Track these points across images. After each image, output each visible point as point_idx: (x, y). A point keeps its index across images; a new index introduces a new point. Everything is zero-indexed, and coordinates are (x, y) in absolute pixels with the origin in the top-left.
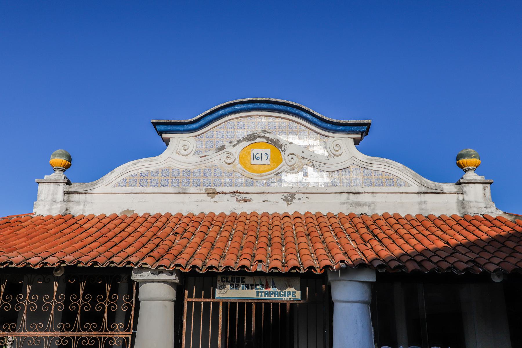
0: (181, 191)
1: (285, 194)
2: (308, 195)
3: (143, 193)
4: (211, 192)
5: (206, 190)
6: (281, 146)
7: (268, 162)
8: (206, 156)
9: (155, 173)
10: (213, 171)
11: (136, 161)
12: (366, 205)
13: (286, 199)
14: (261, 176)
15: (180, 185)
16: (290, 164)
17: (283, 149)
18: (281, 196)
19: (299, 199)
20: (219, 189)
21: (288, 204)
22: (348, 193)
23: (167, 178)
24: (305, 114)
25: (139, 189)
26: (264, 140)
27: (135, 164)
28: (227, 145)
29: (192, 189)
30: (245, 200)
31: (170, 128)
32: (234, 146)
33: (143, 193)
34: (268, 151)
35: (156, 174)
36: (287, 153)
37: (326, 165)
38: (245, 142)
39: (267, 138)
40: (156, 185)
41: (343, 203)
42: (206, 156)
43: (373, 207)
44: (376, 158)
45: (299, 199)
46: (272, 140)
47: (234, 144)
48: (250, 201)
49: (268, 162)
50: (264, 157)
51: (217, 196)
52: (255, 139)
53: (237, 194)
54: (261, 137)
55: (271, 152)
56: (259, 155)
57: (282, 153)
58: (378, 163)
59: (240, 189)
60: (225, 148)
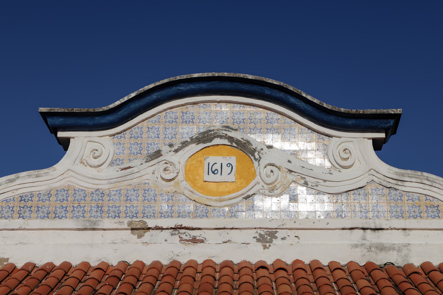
0: (88, 225)
1: (259, 231)
2: (298, 233)
3: (24, 229)
4: (138, 226)
5: (130, 224)
6: (252, 152)
7: (232, 178)
8: (130, 167)
9: (44, 195)
10: (141, 193)
11: (12, 176)
12: (394, 249)
13: (261, 239)
14: (221, 201)
15: (87, 215)
16: (269, 181)
17: (257, 157)
18: (253, 233)
19: (283, 239)
20: (151, 223)
21: (265, 247)
22: (364, 229)
23: (65, 204)
24: (292, 100)
25: (17, 223)
26: (226, 142)
27: (11, 181)
28: (165, 149)
29: (107, 223)
30: (194, 241)
31: (71, 121)
32: (176, 151)
33: (24, 229)
34: (233, 160)
35: (46, 197)
36: (263, 162)
37: (327, 183)
38: (194, 145)
39: (231, 139)
40: (47, 216)
41: (356, 246)
42: (130, 167)
43: (405, 252)
44: (409, 172)
45: (283, 239)
46: (238, 142)
47: (176, 147)
48: (202, 241)
49: (232, 178)
50: (226, 170)
51: (148, 234)
52: (211, 140)
53: (183, 231)
54: (221, 137)
55: (237, 161)
56: (218, 167)
57: (256, 163)
58: (413, 180)
59: (186, 222)
60: (161, 155)
